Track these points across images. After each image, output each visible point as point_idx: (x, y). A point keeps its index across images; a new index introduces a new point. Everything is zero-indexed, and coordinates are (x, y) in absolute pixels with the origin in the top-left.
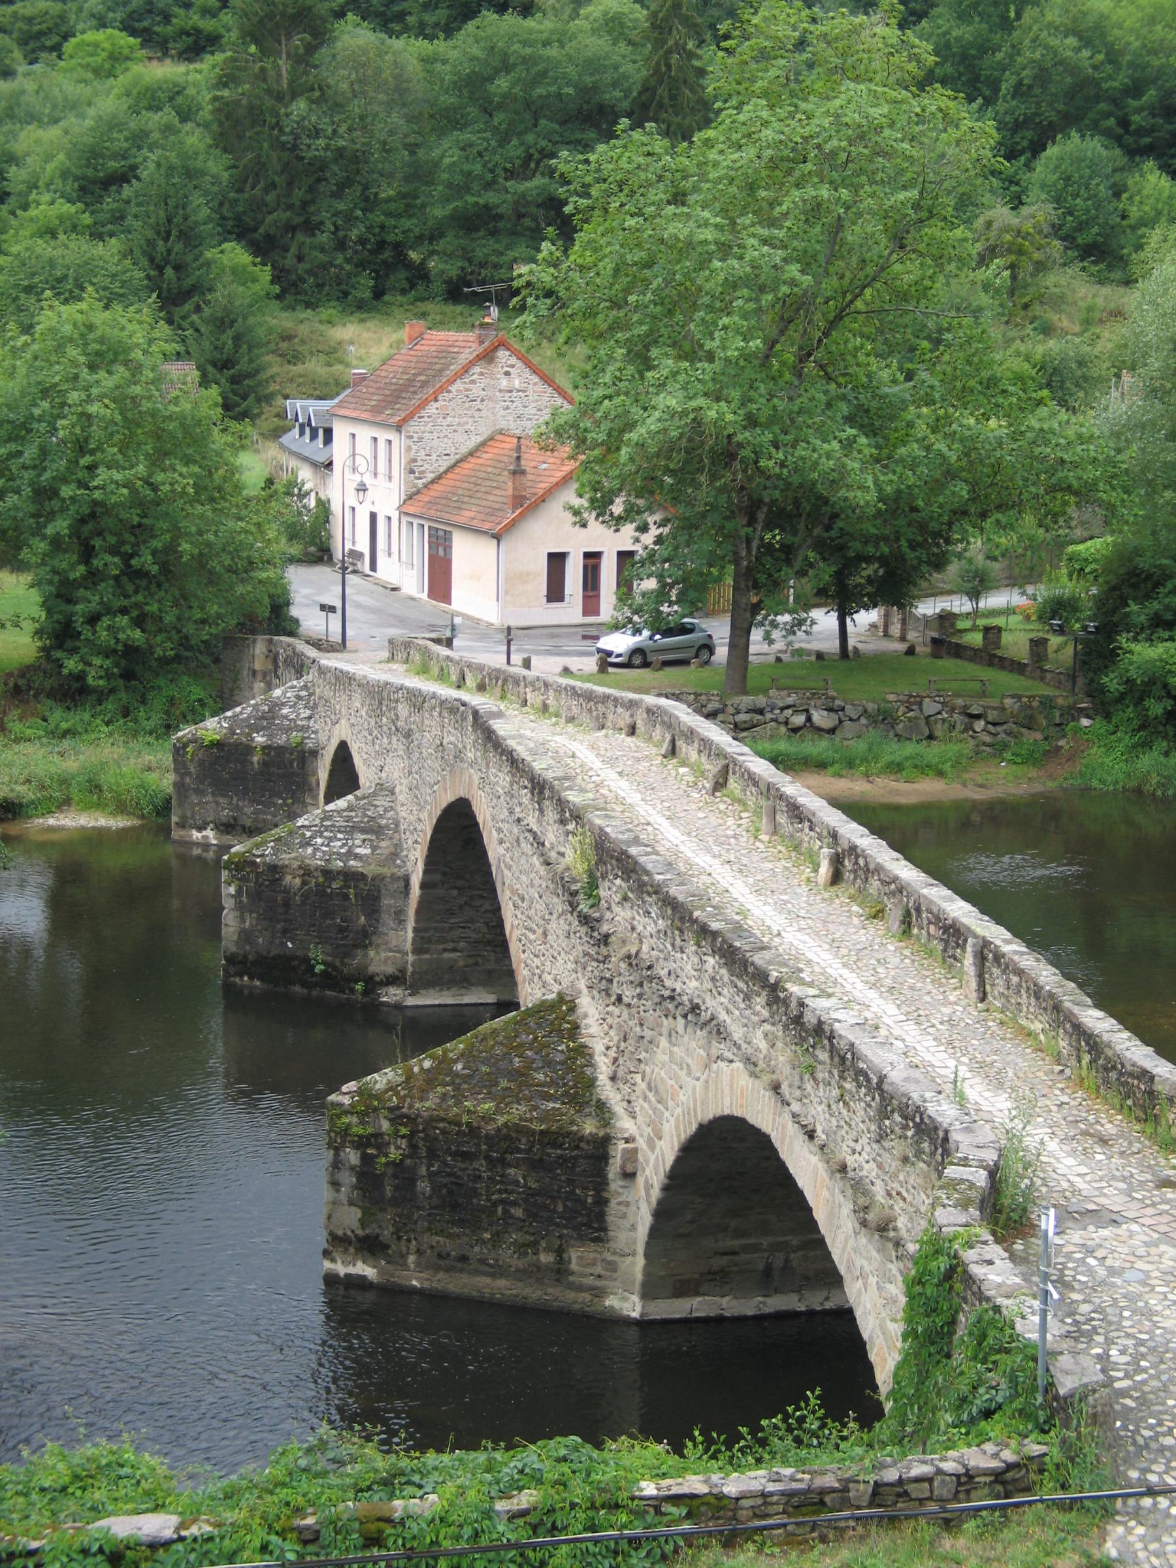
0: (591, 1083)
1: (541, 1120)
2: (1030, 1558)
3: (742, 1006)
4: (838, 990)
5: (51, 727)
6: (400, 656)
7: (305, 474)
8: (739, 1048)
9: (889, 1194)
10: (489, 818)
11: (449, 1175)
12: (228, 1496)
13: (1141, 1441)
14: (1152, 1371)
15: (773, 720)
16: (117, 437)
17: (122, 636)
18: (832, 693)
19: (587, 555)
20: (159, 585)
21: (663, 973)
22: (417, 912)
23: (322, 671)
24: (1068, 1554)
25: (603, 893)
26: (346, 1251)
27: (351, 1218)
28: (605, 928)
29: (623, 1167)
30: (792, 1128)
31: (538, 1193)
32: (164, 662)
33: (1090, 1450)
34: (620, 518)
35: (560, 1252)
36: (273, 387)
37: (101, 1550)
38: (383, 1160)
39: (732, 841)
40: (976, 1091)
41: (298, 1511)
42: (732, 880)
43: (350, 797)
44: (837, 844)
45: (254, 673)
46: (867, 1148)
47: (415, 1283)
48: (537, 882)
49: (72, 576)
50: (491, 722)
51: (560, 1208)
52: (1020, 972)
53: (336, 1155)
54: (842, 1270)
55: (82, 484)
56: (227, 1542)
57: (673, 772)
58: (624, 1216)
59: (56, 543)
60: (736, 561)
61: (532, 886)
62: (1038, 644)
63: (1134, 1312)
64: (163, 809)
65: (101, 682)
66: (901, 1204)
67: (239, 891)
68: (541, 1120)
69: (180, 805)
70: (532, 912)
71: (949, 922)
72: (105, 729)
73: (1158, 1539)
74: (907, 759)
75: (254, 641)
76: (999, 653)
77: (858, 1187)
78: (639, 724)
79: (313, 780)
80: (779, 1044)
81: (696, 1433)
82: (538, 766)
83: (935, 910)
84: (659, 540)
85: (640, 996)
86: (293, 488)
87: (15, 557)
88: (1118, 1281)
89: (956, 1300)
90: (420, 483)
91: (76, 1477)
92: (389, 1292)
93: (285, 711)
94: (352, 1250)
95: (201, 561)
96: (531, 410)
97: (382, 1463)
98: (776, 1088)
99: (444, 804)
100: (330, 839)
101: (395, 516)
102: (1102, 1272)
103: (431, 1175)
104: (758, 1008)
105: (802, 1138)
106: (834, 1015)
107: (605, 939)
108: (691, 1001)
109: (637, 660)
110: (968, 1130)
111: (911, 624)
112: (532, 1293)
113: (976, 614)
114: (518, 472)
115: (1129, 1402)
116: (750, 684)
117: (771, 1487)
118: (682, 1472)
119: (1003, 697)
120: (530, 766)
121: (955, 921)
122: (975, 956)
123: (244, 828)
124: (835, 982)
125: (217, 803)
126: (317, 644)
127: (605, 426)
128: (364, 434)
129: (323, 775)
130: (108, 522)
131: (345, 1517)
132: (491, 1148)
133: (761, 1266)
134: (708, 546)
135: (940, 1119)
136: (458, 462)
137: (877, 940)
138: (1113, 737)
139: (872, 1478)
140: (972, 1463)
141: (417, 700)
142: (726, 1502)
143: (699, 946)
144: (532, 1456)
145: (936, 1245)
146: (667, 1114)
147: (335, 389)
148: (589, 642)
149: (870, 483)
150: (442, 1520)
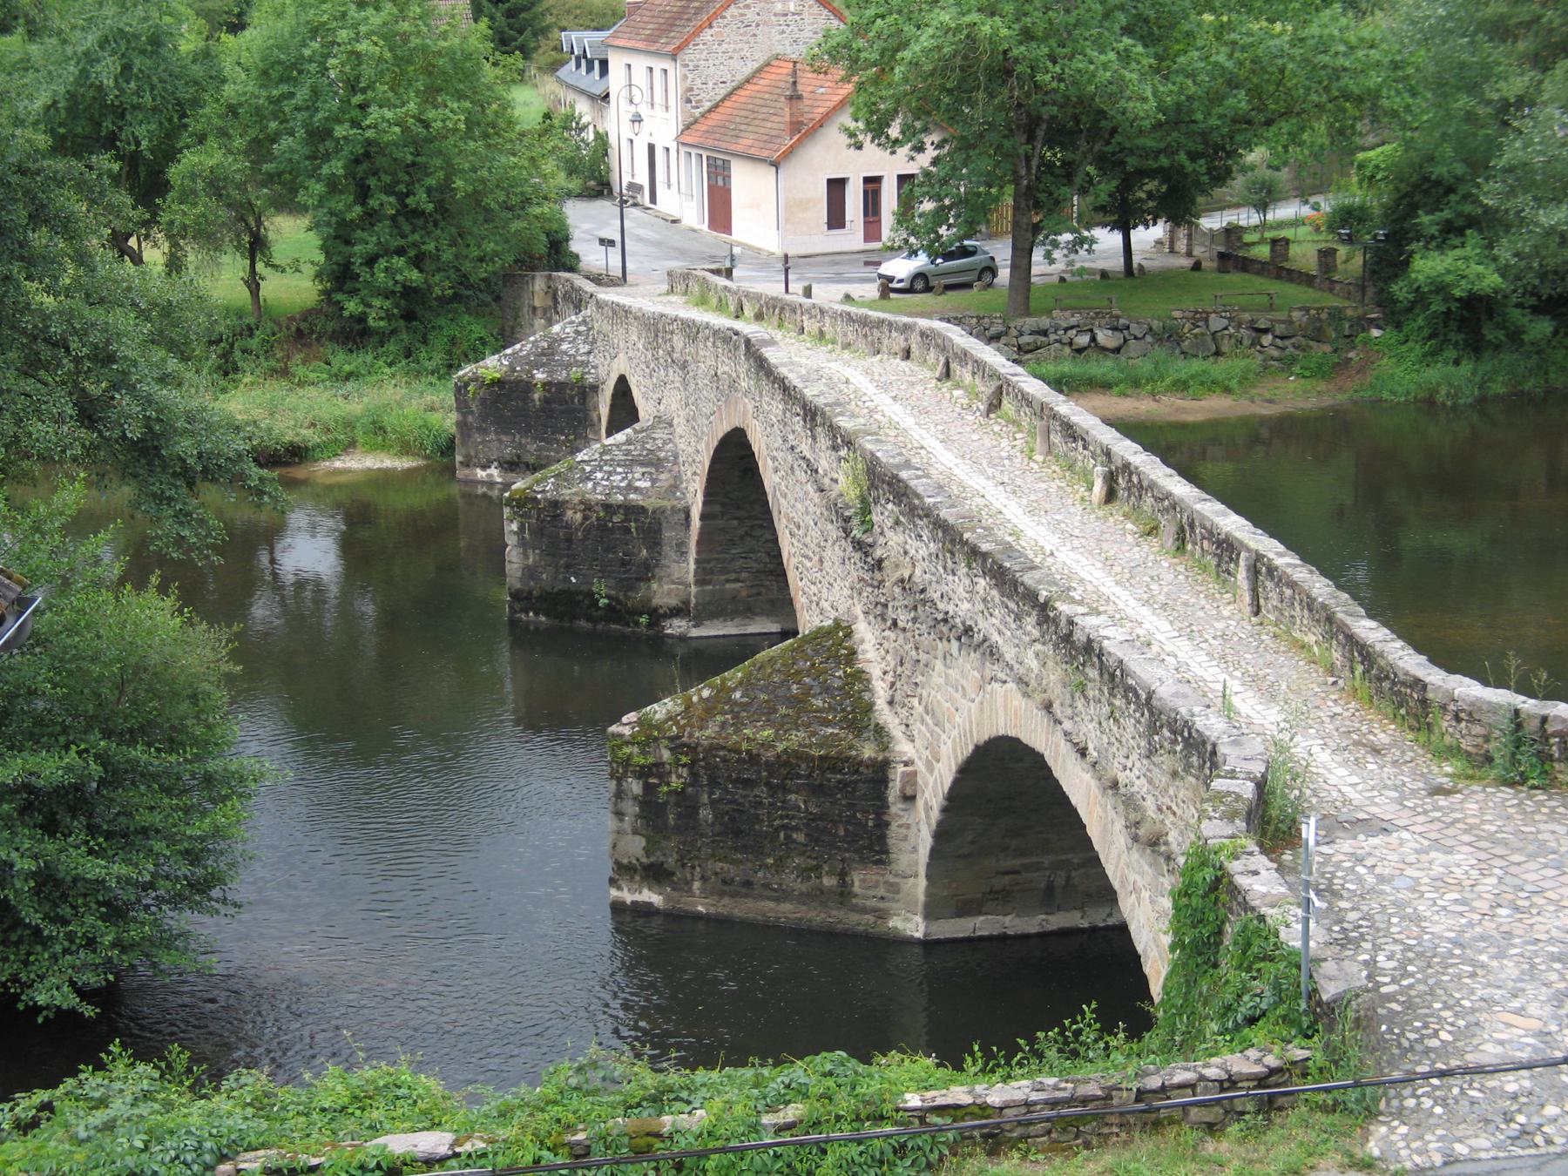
0: (869, 708)
1: (820, 746)
2: (1293, 1159)
3: (1013, 626)
4: (1110, 608)
5: (334, 370)
6: (680, 288)
7: (583, 108)
8: (1011, 669)
9: (1160, 809)
10: (763, 447)
11: (731, 802)
12: (502, 1115)
13: (1406, 1044)
14: (1419, 976)
15: (1056, 341)
16: (387, 78)
17: (399, 277)
18: (1116, 312)
19: (867, 180)
20: (436, 224)
21: (936, 596)
22: (698, 543)
23: (600, 305)
24: (1331, 1154)
25: (875, 518)
26: (632, 878)
27: (635, 847)
28: (878, 553)
29: (902, 790)
30: (1064, 747)
31: (821, 817)
32: (444, 301)
33: (1353, 1052)
34: (896, 141)
35: (843, 875)
36: (549, 20)
37: (379, 1166)
38: (666, 789)
39: (1006, 462)
40: (1246, 703)
41: (570, 1128)
42: (1005, 502)
43: (629, 431)
44: (1110, 461)
45: (534, 309)
46: (1138, 764)
47: (700, 908)
48: (812, 509)
49: (349, 217)
50: (763, 350)
51: (842, 832)
52: (1293, 585)
53: (619, 785)
54: (1116, 885)
55: (355, 124)
56: (500, 1158)
57: (948, 395)
58: (905, 838)
59: (333, 186)
60: (1016, 181)
61: (807, 513)
62: (1326, 255)
63: (1402, 918)
64: (448, 449)
65: (382, 323)
66: (1172, 818)
67: (522, 528)
68: (820, 746)
69: (464, 444)
70: (808, 540)
71: (1222, 537)
72: (387, 370)
73: (1421, 1138)
74: (1192, 377)
75: (533, 278)
76: (1287, 265)
77: (1130, 803)
78: (914, 348)
79: (594, 415)
80: (1050, 664)
81: (976, 1048)
82: (809, 393)
83: (1208, 525)
84: (935, 162)
85: (915, 620)
86: (571, 123)
87: (292, 200)
88: (1387, 888)
89: (1222, 911)
90: (697, 112)
91: (355, 1098)
92: (675, 917)
93: (564, 347)
94: (637, 878)
95: (476, 197)
96: (807, 34)
97: (650, 1080)
98: (1048, 707)
99: (721, 435)
100: (610, 473)
101: (673, 146)
102: (1371, 880)
103: (713, 803)
104: (1029, 628)
105: (1074, 756)
106: (1103, 632)
107: (879, 564)
108: (963, 623)
109: (919, 285)
110: (1236, 743)
111: (1197, 239)
112: (816, 916)
113: (1263, 226)
114: (795, 98)
115: (1395, 1006)
116: (1033, 304)
117: (1034, 1096)
118: (947, 1084)
119: (1291, 310)
120: (801, 392)
121: (1228, 535)
122: (1248, 571)
123: (527, 465)
124: (1108, 600)
125: (500, 441)
126: (597, 280)
127: (879, 45)
128: (640, 64)
129: (605, 409)
130: (381, 162)
131: (615, 1132)
132: (771, 774)
133: (1043, 885)
134: (986, 165)
135: (1207, 733)
136: (735, 89)
137: (1151, 557)
138: (1404, 348)
139: (1135, 1085)
140: (1235, 1069)
141: (692, 331)
142: (989, 1111)
143: (970, 568)
144: (799, 1072)
145: (1202, 856)
146: (944, 737)
147: (613, 20)
148: (870, 268)
149: (1149, 94)
150: (710, 1134)
